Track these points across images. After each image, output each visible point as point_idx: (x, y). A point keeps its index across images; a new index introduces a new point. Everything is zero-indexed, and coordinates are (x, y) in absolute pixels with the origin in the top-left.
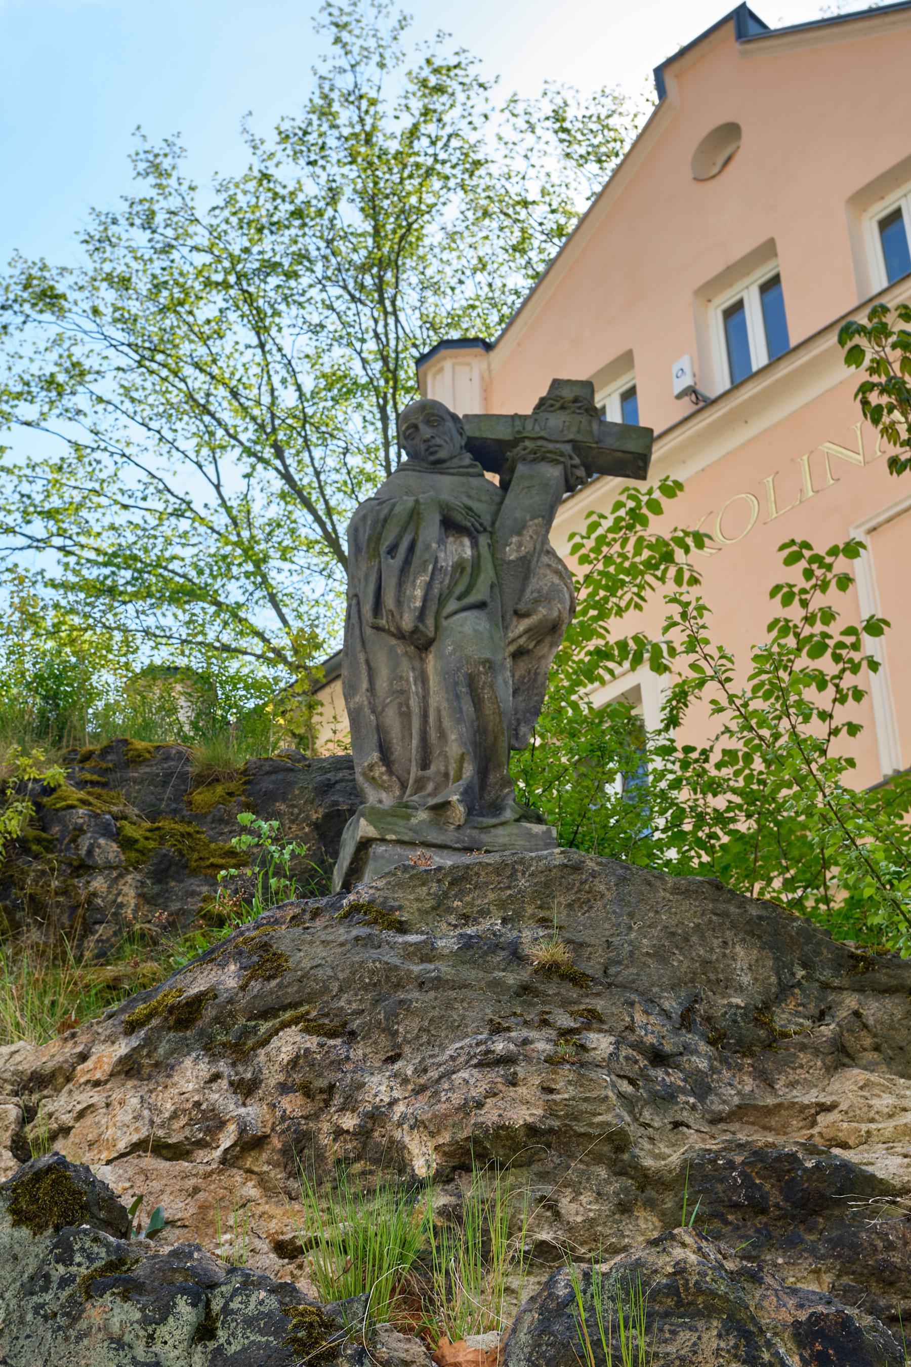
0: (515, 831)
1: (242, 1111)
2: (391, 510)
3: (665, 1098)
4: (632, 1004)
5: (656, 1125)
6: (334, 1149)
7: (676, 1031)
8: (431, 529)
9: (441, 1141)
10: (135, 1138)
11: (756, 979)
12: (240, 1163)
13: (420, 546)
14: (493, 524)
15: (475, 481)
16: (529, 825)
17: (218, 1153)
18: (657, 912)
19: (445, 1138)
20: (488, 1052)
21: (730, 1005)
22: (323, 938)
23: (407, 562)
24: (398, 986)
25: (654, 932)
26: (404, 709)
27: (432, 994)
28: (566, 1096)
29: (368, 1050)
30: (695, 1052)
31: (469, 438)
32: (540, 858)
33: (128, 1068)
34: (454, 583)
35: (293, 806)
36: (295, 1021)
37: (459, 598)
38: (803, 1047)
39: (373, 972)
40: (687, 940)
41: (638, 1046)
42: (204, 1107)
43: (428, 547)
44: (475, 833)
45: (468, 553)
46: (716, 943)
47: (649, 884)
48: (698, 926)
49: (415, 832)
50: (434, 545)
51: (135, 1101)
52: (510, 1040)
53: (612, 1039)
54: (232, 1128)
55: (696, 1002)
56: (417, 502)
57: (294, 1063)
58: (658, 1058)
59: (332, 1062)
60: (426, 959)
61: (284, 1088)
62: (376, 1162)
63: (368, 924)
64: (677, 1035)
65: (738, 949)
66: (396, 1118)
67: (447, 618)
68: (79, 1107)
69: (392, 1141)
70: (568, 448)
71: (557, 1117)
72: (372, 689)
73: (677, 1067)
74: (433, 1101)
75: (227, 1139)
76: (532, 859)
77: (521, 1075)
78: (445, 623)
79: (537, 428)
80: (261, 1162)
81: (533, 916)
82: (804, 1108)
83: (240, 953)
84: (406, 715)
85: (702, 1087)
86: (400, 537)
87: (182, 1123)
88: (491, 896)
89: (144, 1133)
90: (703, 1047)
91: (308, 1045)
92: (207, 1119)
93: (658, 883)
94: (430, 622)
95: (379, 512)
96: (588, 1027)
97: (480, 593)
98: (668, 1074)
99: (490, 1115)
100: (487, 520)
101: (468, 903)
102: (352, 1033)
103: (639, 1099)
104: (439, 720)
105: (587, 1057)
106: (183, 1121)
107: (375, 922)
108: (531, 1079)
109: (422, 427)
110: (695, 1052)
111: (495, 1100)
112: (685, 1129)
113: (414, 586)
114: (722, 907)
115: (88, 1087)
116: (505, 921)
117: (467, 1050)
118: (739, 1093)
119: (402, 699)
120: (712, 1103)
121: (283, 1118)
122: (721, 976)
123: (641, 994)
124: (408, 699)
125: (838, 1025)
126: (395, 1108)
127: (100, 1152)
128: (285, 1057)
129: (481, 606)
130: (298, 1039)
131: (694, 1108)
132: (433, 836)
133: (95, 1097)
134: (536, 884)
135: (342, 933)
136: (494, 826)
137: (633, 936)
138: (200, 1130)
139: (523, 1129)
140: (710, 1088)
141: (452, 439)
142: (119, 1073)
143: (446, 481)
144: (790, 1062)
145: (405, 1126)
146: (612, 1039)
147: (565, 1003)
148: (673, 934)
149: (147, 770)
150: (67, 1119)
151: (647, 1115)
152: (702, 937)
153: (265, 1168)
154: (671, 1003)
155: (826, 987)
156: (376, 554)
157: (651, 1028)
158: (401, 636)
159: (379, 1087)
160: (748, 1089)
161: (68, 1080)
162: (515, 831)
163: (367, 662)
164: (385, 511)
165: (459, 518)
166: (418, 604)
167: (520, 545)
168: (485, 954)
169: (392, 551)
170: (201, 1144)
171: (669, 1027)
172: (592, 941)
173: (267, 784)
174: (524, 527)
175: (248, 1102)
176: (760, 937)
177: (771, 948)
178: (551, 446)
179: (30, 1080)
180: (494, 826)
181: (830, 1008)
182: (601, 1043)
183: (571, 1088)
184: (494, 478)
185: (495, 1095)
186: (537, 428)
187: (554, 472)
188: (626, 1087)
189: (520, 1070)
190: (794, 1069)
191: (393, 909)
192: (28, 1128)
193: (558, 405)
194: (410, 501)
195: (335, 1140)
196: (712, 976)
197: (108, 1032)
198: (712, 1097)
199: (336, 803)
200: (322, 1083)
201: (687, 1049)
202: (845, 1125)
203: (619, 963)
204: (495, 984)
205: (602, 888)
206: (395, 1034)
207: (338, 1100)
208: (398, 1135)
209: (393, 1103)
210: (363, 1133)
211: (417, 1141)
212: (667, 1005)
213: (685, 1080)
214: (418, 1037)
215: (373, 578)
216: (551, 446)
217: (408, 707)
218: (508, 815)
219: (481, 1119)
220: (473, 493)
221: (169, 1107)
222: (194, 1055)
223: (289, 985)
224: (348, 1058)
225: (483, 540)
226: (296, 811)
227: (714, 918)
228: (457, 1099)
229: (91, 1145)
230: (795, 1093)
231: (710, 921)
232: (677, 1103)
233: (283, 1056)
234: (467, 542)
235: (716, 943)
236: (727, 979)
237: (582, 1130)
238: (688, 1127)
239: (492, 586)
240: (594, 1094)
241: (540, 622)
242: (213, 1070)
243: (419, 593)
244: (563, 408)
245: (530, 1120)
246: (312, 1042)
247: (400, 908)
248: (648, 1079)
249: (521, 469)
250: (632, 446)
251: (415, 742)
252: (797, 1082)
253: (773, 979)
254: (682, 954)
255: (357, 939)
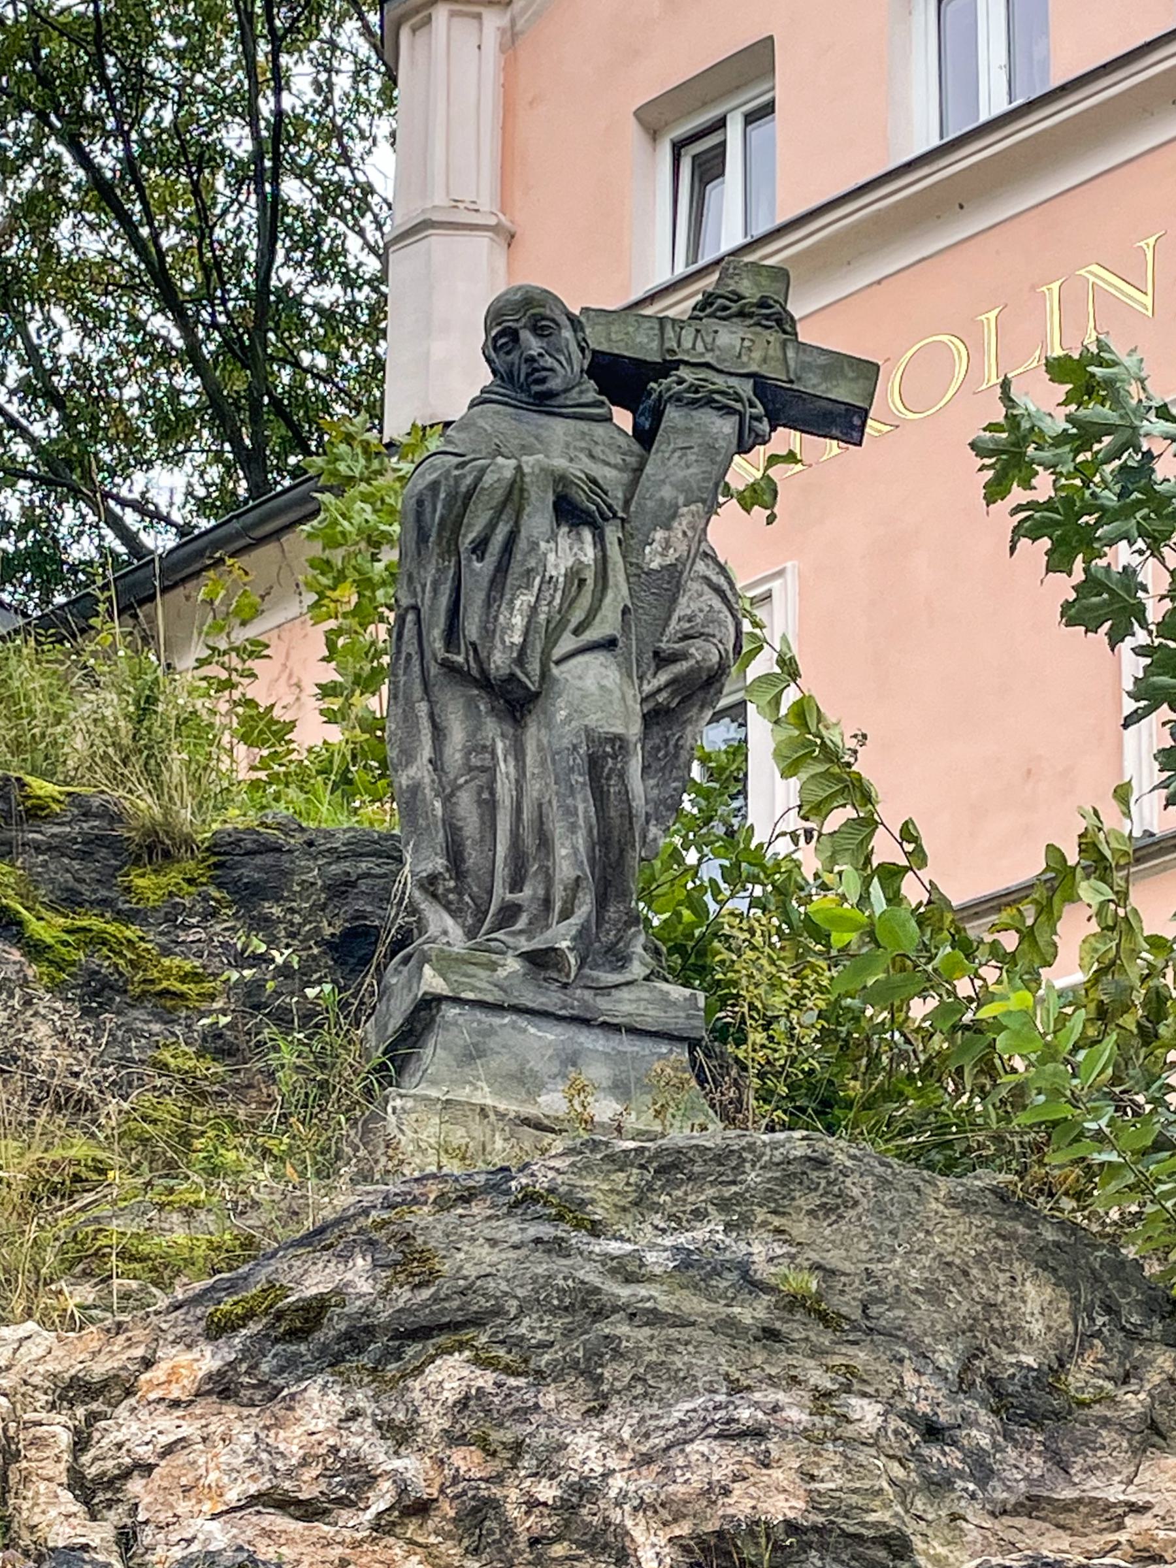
0: (646, 995)
1: (397, 1464)
2: (479, 479)
3: (938, 1485)
4: (901, 1361)
5: (930, 1517)
6: (527, 1525)
7: (952, 1395)
8: (538, 519)
9: (677, 1532)
10: (253, 1489)
11: (1049, 1328)
12: (398, 1530)
13: (522, 544)
14: (627, 503)
15: (599, 430)
16: (665, 986)
17: (369, 1515)
18: (928, 1232)
19: (683, 1529)
20: (730, 1421)
21: (1019, 1365)
22: (488, 1233)
23: (502, 568)
24: (599, 1314)
25: (926, 1261)
26: (485, 796)
27: (647, 1331)
28: (832, 1486)
29: (562, 1396)
30: (975, 1424)
31: (595, 353)
32: (775, 1145)
33: (221, 1388)
34: (569, 603)
35: (292, 910)
36: (461, 1346)
37: (576, 632)
38: (1105, 1422)
39: (562, 1291)
40: (966, 1274)
41: (909, 1416)
42: (343, 1453)
43: (534, 546)
44: (588, 995)
45: (589, 554)
46: (1003, 1278)
47: (918, 1190)
48: (979, 1254)
49: (501, 988)
50: (543, 545)
51: (247, 1439)
52: (756, 1405)
53: (879, 1408)
54: (385, 1485)
55: (976, 1357)
56: (519, 468)
57: (463, 1403)
58: (933, 1431)
59: (516, 1411)
60: (630, 1279)
61: (455, 1439)
62: (581, 1545)
63: (550, 1219)
64: (954, 1401)
65: (1028, 1286)
66: (613, 1494)
67: (558, 663)
68: (164, 1440)
69: (607, 1522)
70: (746, 388)
71: (822, 1511)
72: (436, 763)
73: (954, 1443)
74: (663, 1479)
75: (381, 1498)
76: (765, 1145)
77: (775, 1454)
78: (555, 671)
79: (700, 347)
80: (426, 1533)
81: (764, 1224)
82: (1109, 1506)
83: (372, 1243)
84: (489, 806)
85: (982, 1469)
86: (492, 526)
87: (314, 1473)
88: (711, 1192)
89: (264, 1484)
90: (984, 1417)
91: (480, 1383)
92: (350, 1471)
93: (929, 1190)
94: (534, 667)
95: (457, 479)
96: (847, 1389)
97: (606, 625)
98: (944, 1454)
99: (740, 1504)
100: (617, 497)
101: (678, 1199)
102: (539, 1373)
103: (912, 1485)
104: (541, 819)
105: (849, 1431)
106: (315, 1470)
107: (560, 1217)
108: (789, 1460)
109: (526, 335)
110: (975, 1424)
111: (744, 1485)
112: (964, 1524)
113: (512, 609)
114: (1008, 1225)
115: (162, 1408)
116: (729, 1227)
117: (702, 1414)
118: (1026, 1478)
119: (483, 779)
120: (994, 1490)
121: (455, 1480)
122: (1006, 1323)
123: (911, 1346)
124: (494, 780)
125: (1150, 1395)
126: (610, 1481)
127: (199, 1501)
128: (450, 1395)
129: (609, 644)
130: (465, 1373)
131: (973, 1496)
132: (530, 998)
133: (169, 1426)
134: (769, 1180)
135: (513, 1229)
136: (616, 986)
137: (898, 1262)
138: (341, 1484)
139: (782, 1526)
140: (992, 1471)
141: (569, 360)
142: (209, 1393)
143: (559, 429)
144: (1088, 1443)
145: (627, 1507)
146: (879, 1408)
147: (816, 1352)
148: (949, 1264)
149: (56, 830)
150: (145, 1453)
151: (919, 1504)
152: (985, 1269)
153: (433, 1539)
154: (945, 1358)
155: (1132, 1335)
156: (451, 548)
157: (925, 1392)
158: (484, 682)
159: (586, 1451)
160: (1037, 1473)
161: (129, 1393)
162: (646, 995)
163: (432, 716)
164: (469, 480)
165: (580, 498)
166: (517, 639)
167: (667, 544)
168: (709, 1276)
169: (480, 547)
170: (343, 1502)
171: (945, 1391)
172: (847, 1267)
173: (249, 872)
174: (674, 516)
175: (402, 1450)
176: (1054, 1270)
177: (1068, 1287)
178: (720, 381)
179: (70, 1387)
180: (616, 986)
181: (1136, 1368)
182: (866, 1413)
183: (837, 1475)
184: (623, 418)
185: (745, 1479)
186: (700, 347)
187: (726, 427)
188: (898, 1471)
189: (773, 1446)
190: (1094, 1450)
191: (583, 1203)
192: (85, 1459)
193: (735, 307)
194: (506, 466)
195: (528, 1513)
196: (996, 1323)
197: (179, 1331)
198: (994, 1482)
199: (360, 915)
200: (508, 1436)
201: (966, 1420)
202: (1162, 1534)
203: (882, 1301)
204: (729, 1326)
205: (856, 1192)
206: (600, 1379)
207: (528, 1462)
208: (616, 1516)
209: (608, 1474)
210: (567, 1508)
211: (643, 1525)
212: (941, 1360)
213: (962, 1461)
214: (629, 1387)
215: (446, 589)
216: (720, 381)
217: (492, 793)
218: (637, 970)
219: (730, 1511)
220: (597, 451)
221: (296, 1452)
222: (320, 1381)
223: (447, 1298)
224: (537, 1406)
225: (612, 533)
226: (297, 919)
227: (1000, 1244)
228: (697, 1481)
229: (186, 1490)
230: (1093, 1481)
231: (996, 1249)
232: (954, 1490)
233: (446, 1394)
234: (587, 535)
235: (1003, 1278)
236: (1014, 1327)
237: (851, 1530)
238: (966, 1521)
239: (625, 611)
240: (866, 1484)
241: (691, 670)
242: (349, 1405)
243: (518, 621)
244: (741, 314)
245: (791, 1515)
246: (486, 1379)
247: (592, 1201)
248: (922, 1460)
249: (672, 415)
250: (843, 392)
251: (502, 850)
252: (1097, 1467)
253: (1069, 1328)
254: (961, 1293)
255: (538, 1241)
